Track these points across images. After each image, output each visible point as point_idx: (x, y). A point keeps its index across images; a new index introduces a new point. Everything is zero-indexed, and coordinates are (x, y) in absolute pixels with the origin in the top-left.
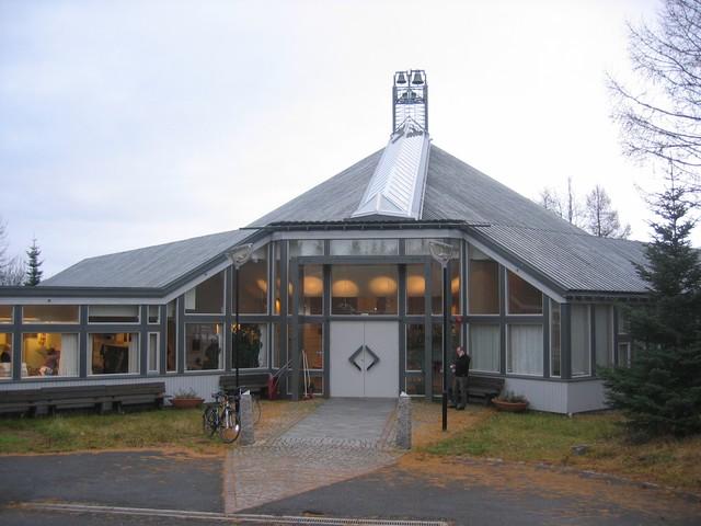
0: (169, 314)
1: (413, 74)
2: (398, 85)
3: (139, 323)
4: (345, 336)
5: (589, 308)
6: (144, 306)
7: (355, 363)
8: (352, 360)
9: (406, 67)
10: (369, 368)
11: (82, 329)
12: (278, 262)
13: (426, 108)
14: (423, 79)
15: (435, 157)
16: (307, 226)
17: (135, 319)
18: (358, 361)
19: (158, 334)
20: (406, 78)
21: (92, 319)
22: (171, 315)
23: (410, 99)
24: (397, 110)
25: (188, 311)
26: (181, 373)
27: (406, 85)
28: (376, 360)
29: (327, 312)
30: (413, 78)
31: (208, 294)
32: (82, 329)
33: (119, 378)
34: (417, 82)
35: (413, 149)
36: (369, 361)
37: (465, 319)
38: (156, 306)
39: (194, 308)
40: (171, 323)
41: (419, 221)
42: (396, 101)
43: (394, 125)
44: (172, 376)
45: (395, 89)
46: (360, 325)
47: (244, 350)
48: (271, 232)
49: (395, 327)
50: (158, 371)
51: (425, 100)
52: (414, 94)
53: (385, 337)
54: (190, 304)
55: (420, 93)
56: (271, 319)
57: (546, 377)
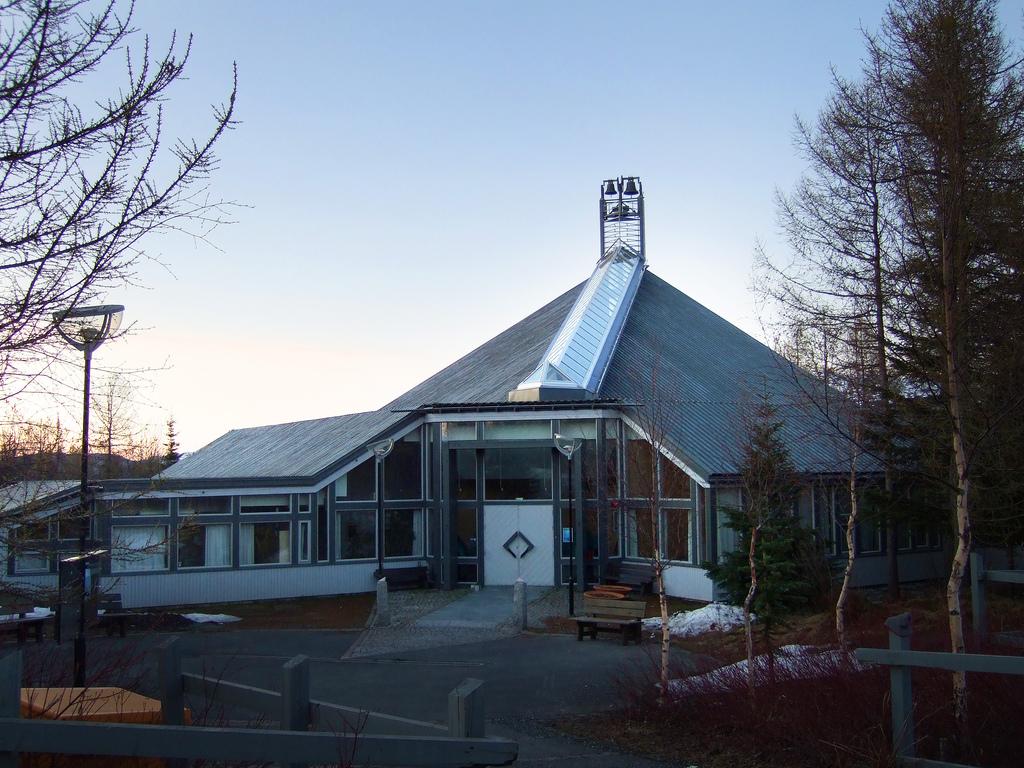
0: (320, 502)
1: (626, 182)
2: (607, 197)
3: (310, 512)
4: (501, 520)
5: (740, 491)
6: (295, 495)
7: (509, 551)
8: (507, 546)
9: (614, 175)
10: (522, 556)
11: (235, 519)
12: (431, 444)
13: (642, 225)
14: (638, 189)
15: (650, 292)
16: (242, 484)
17: (285, 508)
18: (513, 547)
19: (309, 522)
20: (616, 189)
21: (245, 509)
22: (322, 503)
23: (622, 214)
24: (606, 229)
25: (340, 498)
26: (332, 562)
27: (616, 196)
28: (531, 547)
29: (480, 498)
30: (625, 188)
31: (360, 479)
32: (235, 519)
33: (397, 560)
34: (632, 191)
35: (623, 277)
36: (523, 547)
37: (622, 503)
38: (305, 495)
39: (346, 495)
40: (322, 509)
41: (535, 403)
42: (604, 217)
43: (603, 248)
44: (324, 564)
45: (603, 203)
46: (515, 507)
47: (399, 539)
48: (417, 412)
49: (550, 508)
50: (48, 569)
51: (640, 213)
52: (627, 208)
53: (536, 520)
54: (342, 490)
55: (634, 206)
56: (424, 504)
57: (173, 570)
